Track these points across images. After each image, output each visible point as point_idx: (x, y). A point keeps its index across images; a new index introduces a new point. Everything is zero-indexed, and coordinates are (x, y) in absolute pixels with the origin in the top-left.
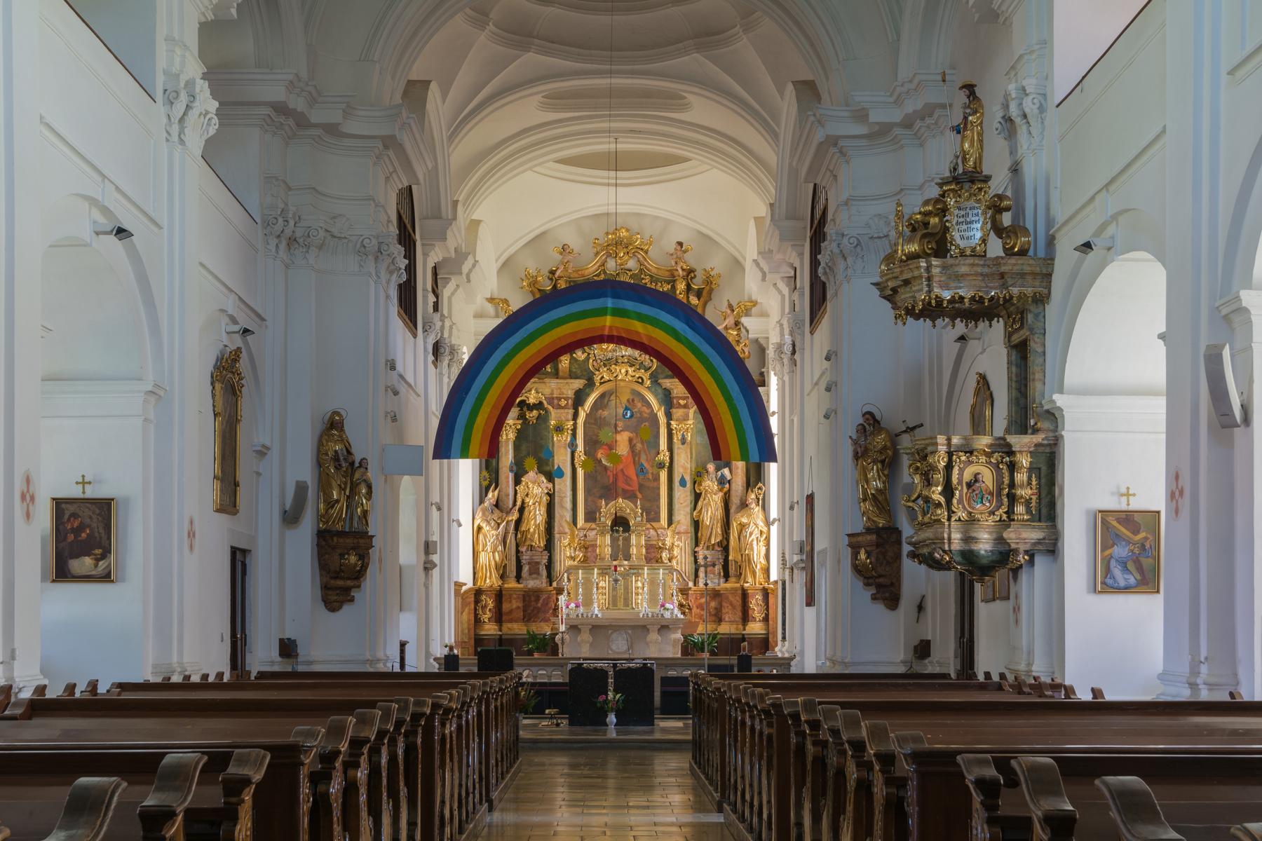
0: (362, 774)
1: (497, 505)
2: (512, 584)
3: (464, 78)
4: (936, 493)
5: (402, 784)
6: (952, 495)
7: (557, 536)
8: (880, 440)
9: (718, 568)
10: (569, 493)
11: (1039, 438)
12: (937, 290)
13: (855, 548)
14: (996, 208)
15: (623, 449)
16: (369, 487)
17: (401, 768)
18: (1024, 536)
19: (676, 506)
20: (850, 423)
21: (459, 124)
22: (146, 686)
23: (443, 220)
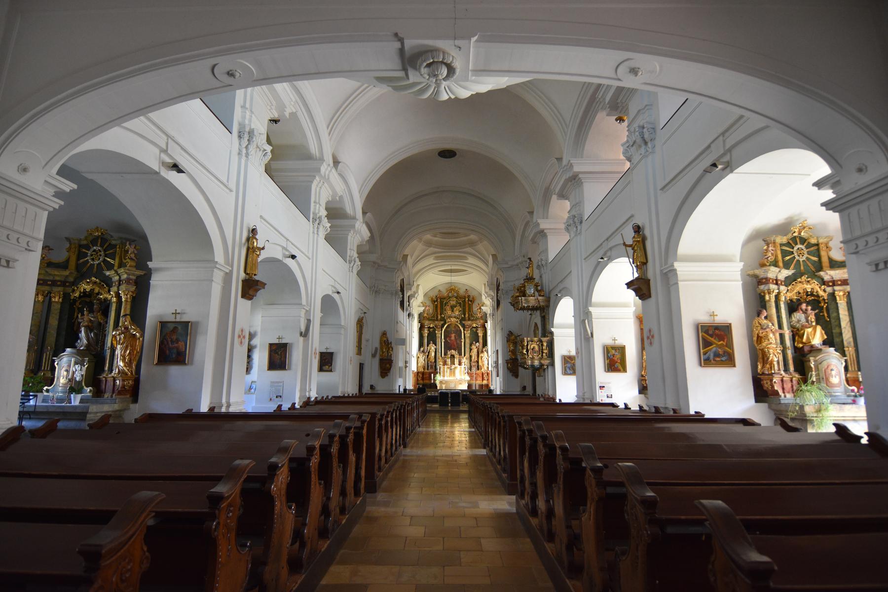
0: (389, 419)
3: (416, 253)
4: (525, 351)
5: (351, 452)
8: (513, 337)
13: (507, 363)
14: (536, 286)
15: (453, 338)
17: (365, 438)
18: (546, 362)
21: (414, 265)
22: (339, 397)
23: (410, 285)
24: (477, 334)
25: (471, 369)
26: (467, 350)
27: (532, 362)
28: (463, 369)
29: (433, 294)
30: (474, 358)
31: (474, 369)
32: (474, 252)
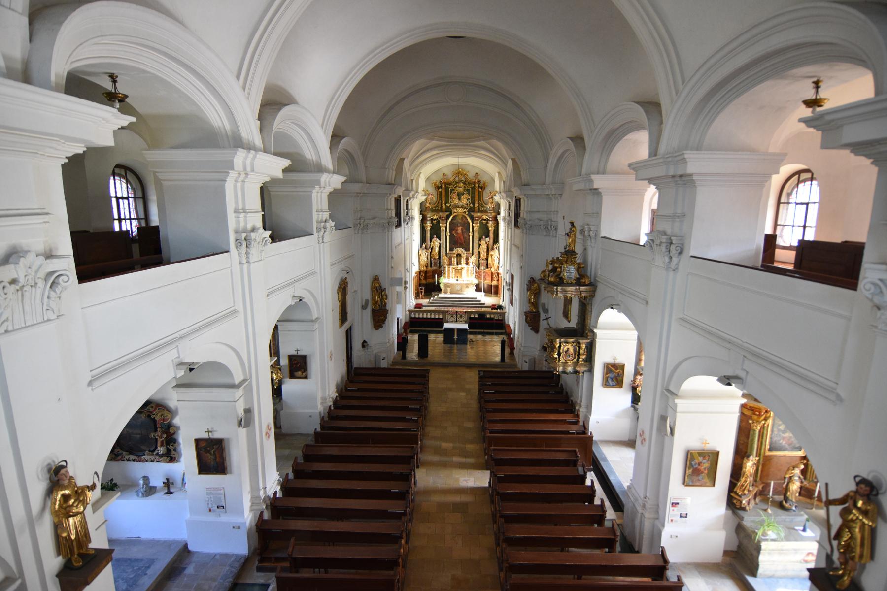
2: (429, 269)
15: (460, 231)
20: (527, 279)
25: (479, 267)
26: (476, 245)
29: (437, 179)
30: (483, 255)
31: (482, 268)
32: (488, 146)
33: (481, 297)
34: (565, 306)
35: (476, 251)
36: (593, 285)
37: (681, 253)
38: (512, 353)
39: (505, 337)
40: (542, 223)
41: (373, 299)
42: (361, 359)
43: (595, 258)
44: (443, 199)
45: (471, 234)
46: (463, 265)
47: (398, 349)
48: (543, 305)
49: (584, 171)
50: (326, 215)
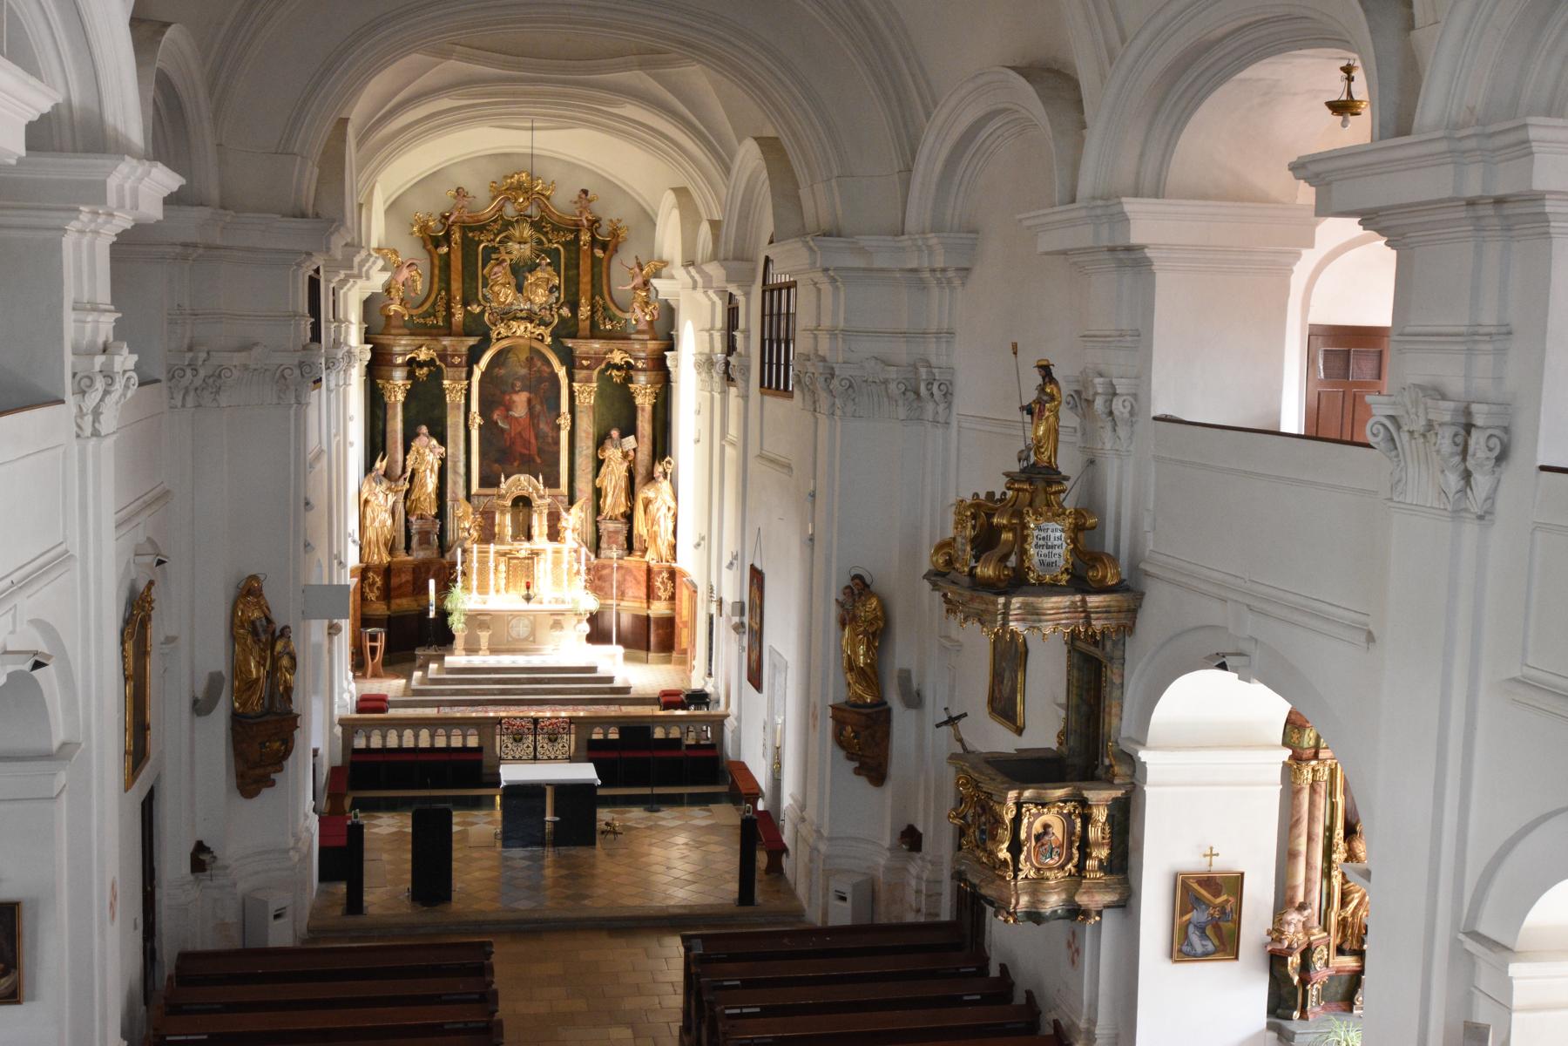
1: (385, 475)
2: (402, 556)
4: (1004, 854)
6: (1020, 851)
7: (449, 503)
9: (622, 538)
10: (462, 457)
11: (1119, 793)
12: (1013, 625)
16: (293, 659)
19: (578, 473)
24: (629, 399)
27: (1036, 901)
28: (566, 557)
29: (429, 208)
30: (614, 502)
31: (612, 553)
33: (611, 661)
34: (997, 677)
35: (584, 487)
36: (1130, 592)
37: (1502, 457)
38: (775, 867)
39: (728, 815)
40: (892, 373)
41: (238, 669)
42: (195, 919)
43: (1130, 488)
44: (456, 286)
45: (564, 421)
46: (540, 540)
47: (323, 877)
48: (905, 677)
49: (1085, 187)
50: (105, 325)
